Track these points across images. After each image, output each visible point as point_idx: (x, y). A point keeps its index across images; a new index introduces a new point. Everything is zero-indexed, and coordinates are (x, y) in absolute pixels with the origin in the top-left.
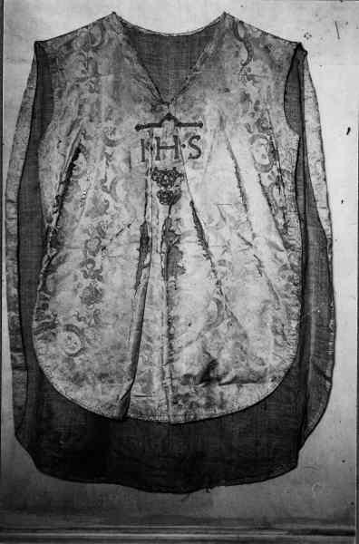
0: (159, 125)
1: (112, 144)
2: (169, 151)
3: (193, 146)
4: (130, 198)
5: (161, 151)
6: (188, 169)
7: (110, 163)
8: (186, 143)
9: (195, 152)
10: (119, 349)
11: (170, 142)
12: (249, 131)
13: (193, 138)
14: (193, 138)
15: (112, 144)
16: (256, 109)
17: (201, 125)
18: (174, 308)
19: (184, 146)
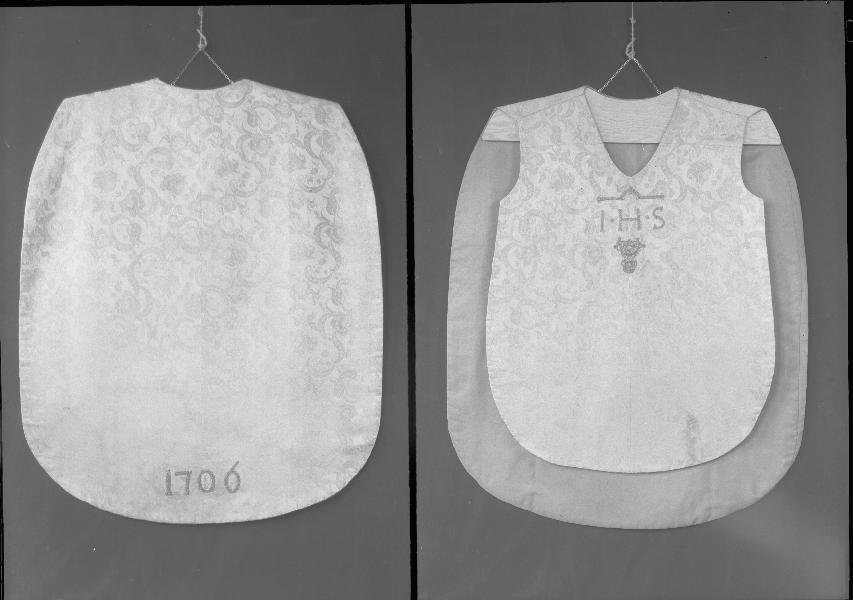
0: (621, 198)
1: (573, 212)
2: (632, 223)
3: (656, 217)
4: (587, 265)
5: (624, 222)
6: (649, 238)
7: (165, 130)
8: (650, 214)
9: (658, 223)
10: (122, 188)
11: (633, 215)
12: (191, 112)
13: (657, 209)
14: (657, 209)
15: (573, 212)
16: (719, 177)
17: (662, 197)
18: (342, 267)
19: (648, 217)
